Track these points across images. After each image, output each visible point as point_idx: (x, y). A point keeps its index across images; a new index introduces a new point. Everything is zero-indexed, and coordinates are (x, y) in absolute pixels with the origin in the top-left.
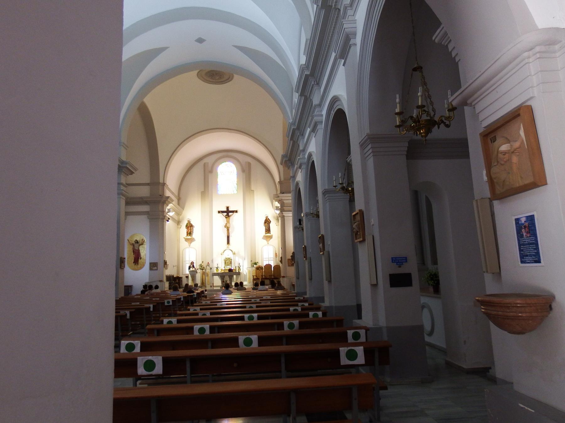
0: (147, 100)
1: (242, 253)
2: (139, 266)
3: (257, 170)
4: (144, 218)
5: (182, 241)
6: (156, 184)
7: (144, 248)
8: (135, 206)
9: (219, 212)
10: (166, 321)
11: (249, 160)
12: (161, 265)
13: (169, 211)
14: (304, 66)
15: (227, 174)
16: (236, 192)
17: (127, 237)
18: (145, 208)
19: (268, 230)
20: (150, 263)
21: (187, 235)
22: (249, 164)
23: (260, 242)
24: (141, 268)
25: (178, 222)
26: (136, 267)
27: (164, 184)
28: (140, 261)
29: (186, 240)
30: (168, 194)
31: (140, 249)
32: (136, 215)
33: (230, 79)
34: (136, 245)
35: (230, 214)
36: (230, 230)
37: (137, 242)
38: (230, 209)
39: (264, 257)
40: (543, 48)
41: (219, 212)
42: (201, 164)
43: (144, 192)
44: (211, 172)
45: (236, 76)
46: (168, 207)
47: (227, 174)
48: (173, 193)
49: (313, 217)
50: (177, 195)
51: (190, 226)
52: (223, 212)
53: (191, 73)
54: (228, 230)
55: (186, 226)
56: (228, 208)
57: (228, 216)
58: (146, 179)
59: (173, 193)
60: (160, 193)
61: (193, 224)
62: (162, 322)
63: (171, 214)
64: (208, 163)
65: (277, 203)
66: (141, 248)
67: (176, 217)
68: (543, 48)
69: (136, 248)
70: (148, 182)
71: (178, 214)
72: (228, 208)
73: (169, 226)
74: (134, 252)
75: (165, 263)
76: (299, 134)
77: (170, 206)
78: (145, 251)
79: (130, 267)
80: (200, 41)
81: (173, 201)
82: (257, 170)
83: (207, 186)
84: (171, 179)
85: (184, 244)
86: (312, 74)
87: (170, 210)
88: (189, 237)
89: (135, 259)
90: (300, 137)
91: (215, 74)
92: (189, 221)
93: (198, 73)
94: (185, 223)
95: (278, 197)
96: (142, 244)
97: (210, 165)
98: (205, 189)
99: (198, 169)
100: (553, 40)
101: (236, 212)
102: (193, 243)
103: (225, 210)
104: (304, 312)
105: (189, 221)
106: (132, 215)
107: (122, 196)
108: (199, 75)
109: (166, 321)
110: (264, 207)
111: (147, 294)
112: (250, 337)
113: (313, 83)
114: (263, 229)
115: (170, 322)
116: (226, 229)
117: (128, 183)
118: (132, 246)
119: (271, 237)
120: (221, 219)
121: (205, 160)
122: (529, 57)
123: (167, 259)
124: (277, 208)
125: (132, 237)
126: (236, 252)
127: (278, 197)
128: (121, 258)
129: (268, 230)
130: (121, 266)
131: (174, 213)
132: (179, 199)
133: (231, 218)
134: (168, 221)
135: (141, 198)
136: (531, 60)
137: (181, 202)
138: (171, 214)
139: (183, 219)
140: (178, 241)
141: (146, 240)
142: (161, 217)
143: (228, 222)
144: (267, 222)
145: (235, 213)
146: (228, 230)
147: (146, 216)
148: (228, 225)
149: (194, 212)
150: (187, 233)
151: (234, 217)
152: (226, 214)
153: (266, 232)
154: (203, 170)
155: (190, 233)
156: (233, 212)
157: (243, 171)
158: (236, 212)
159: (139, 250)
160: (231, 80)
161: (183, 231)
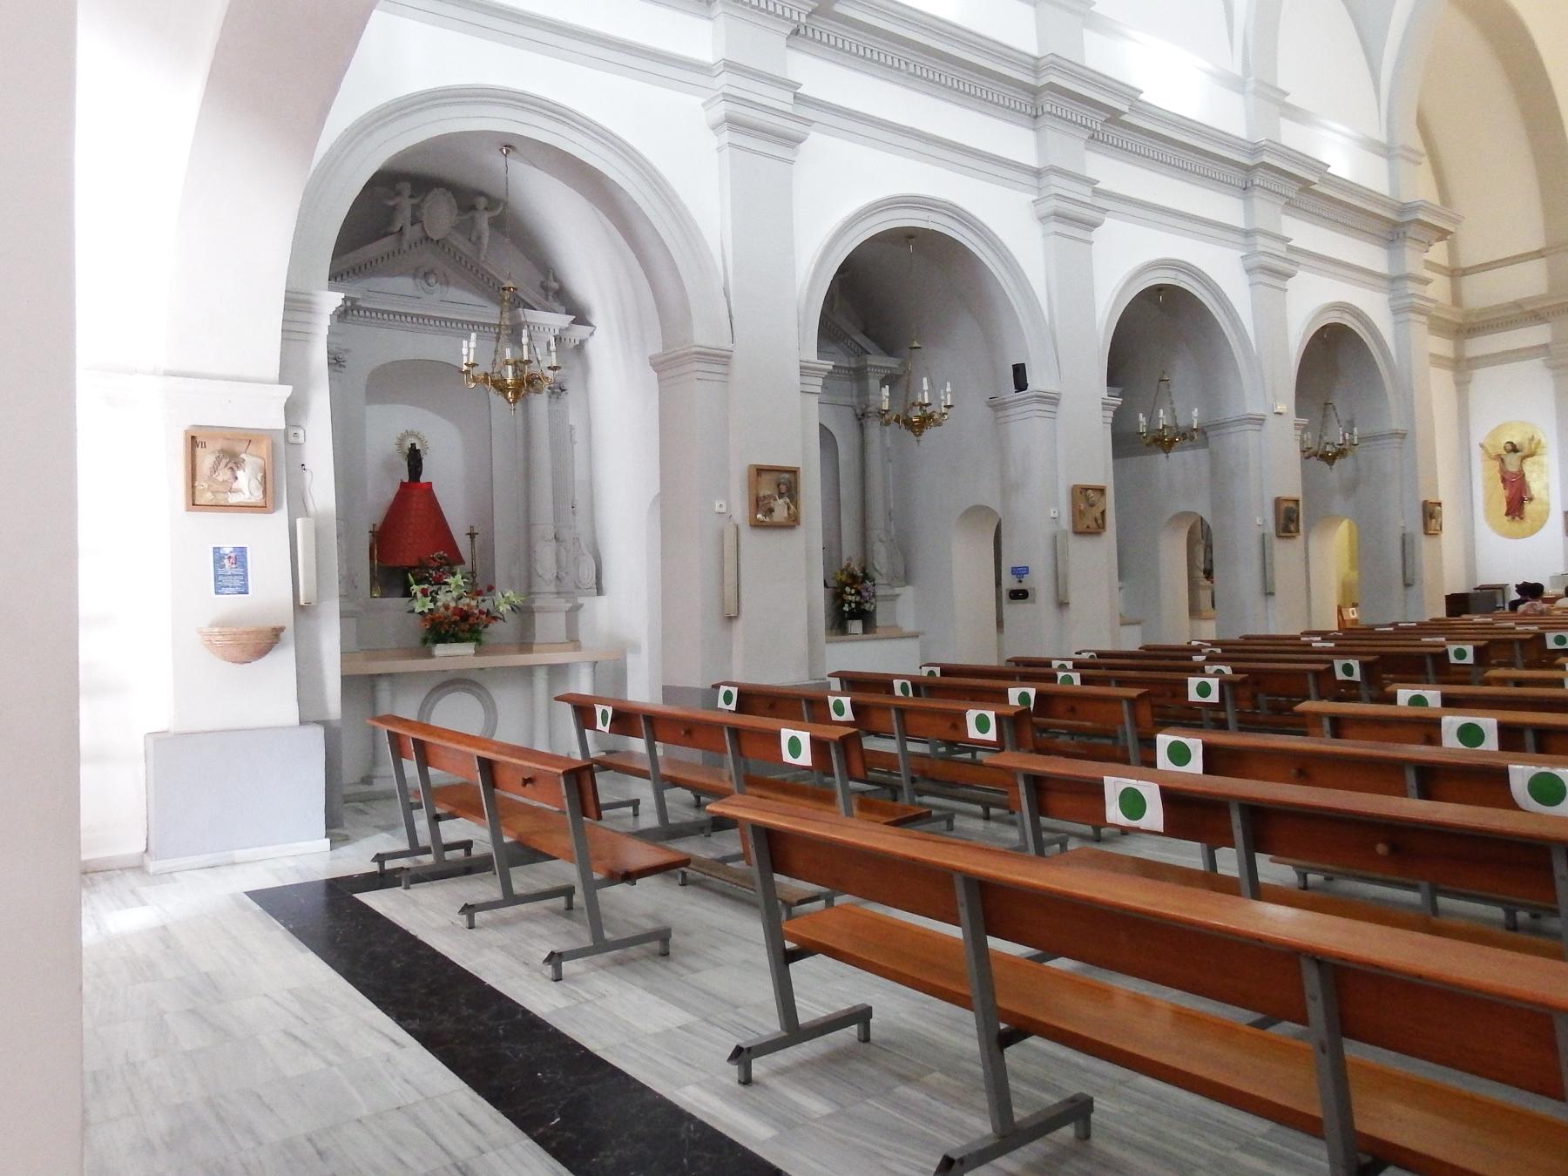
7: (1541, 465)
10: (1404, 694)
18: (1537, 335)
24: (1533, 531)
26: (1516, 526)
28: (1528, 507)
37: (1514, 449)
49: (920, 423)
62: (1392, 699)
66: (1528, 467)
70: (1535, 246)
74: (1504, 480)
79: (1494, 527)
89: (1509, 503)
96: (1532, 455)
104: (946, 680)
109: (1404, 694)
111: (1525, 614)
112: (1462, 746)
115: (1418, 701)
117: (274, 371)
118: (1497, 463)
130: (1425, 525)
147: (1538, 362)
159: (1521, 476)
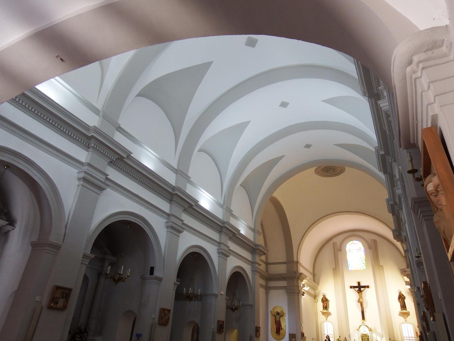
0: (276, 194)
1: (379, 330)
2: (281, 336)
3: (382, 246)
4: (283, 292)
5: (320, 314)
6: (292, 262)
7: (284, 319)
8: (278, 282)
9: (351, 287)
11: (375, 237)
12: (299, 336)
13: (304, 286)
14: (378, 148)
15: (355, 252)
16: (365, 268)
17: (270, 309)
18: (283, 283)
19: (403, 306)
20: (290, 334)
21: (324, 309)
22: (375, 241)
23: (397, 319)
25: (315, 297)
27: (297, 262)
28: (281, 331)
29: (323, 313)
30: (301, 270)
31: (281, 320)
32: (279, 289)
33: (342, 171)
34: (278, 317)
35: (362, 289)
36: (364, 306)
37: (278, 314)
38: (362, 284)
39: (405, 336)
40: (423, 56)
41: (351, 287)
42: (331, 243)
43: (282, 269)
44: (340, 250)
45: (347, 168)
46: (303, 283)
47: (355, 252)
48: (307, 270)
50: (312, 271)
51: (325, 300)
52: (355, 287)
53: (308, 170)
54: (362, 305)
55: (322, 300)
56: (359, 283)
57: (360, 291)
58: (282, 258)
59: (307, 270)
60: (295, 270)
61: (328, 299)
63: (306, 288)
64: (336, 242)
65: (406, 277)
67: (312, 292)
68: (423, 56)
69: (278, 320)
70: (285, 261)
71: (314, 288)
72: (359, 283)
73: (305, 300)
74: (276, 323)
75: (303, 335)
76: (398, 208)
77: (304, 282)
78: (285, 324)
80: (308, 146)
81: (306, 277)
82: (382, 246)
83: (338, 264)
84: (305, 257)
85: (321, 318)
86: (387, 153)
87: (305, 286)
88: (326, 311)
89: (277, 329)
90: (400, 212)
91: (329, 169)
92: (324, 296)
93: (316, 170)
94: (321, 297)
95: (405, 271)
96: (282, 316)
97: (338, 244)
98: (336, 266)
99: (328, 250)
100: (432, 44)
101: (368, 287)
102: (329, 317)
103: (357, 285)
105: (324, 296)
106: (273, 289)
107: (256, 273)
108: (317, 172)
110: (396, 283)
113: (390, 161)
114: (397, 305)
116: (359, 304)
118: (274, 317)
119: (408, 314)
120: (352, 295)
121: (334, 240)
122: (414, 72)
123: (304, 331)
124: (407, 283)
125: (275, 308)
126: (372, 329)
127: (405, 271)
128: (256, 327)
129: (403, 306)
131: (308, 288)
132: (314, 275)
133: (363, 293)
134: (303, 295)
135: (280, 275)
136: (419, 74)
137: (316, 279)
138: (306, 288)
139: (319, 294)
140: (316, 314)
141: (286, 311)
142: (296, 291)
143: (361, 297)
144: (401, 298)
145: (366, 289)
146: (362, 305)
148: (361, 300)
149: (328, 288)
150: (323, 307)
151: (367, 293)
152: (358, 289)
153: (401, 308)
154: (333, 250)
155: (326, 307)
156: (364, 287)
157: (370, 248)
158: (368, 287)
160: (344, 172)
161: (320, 305)
